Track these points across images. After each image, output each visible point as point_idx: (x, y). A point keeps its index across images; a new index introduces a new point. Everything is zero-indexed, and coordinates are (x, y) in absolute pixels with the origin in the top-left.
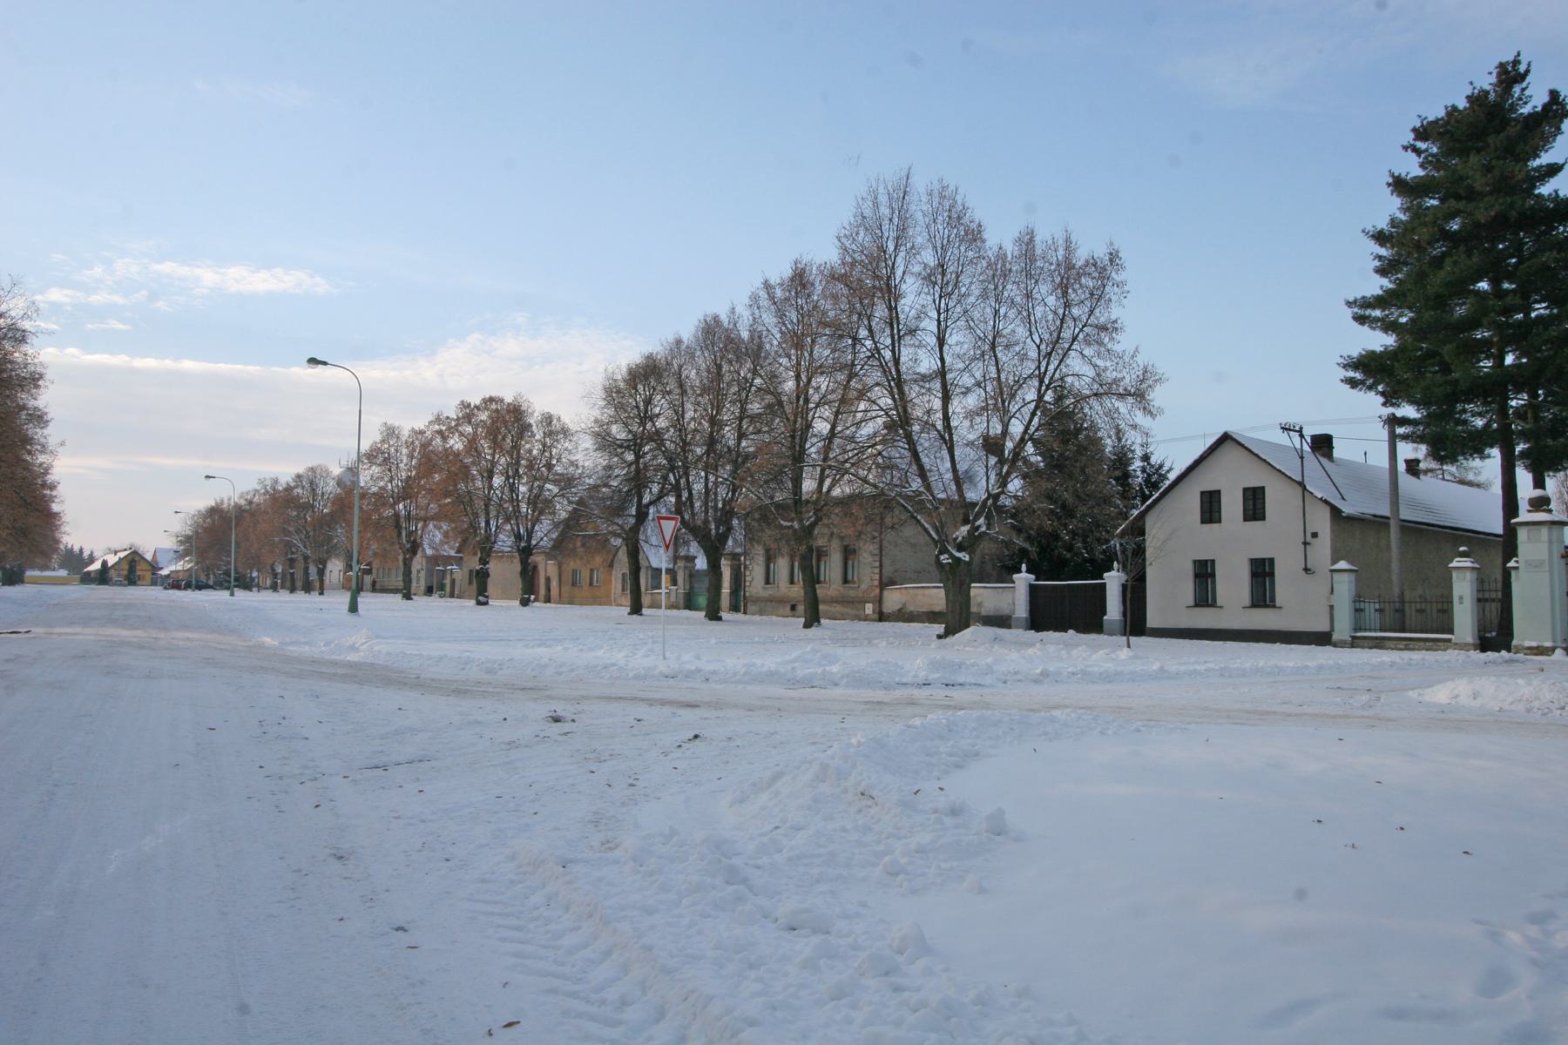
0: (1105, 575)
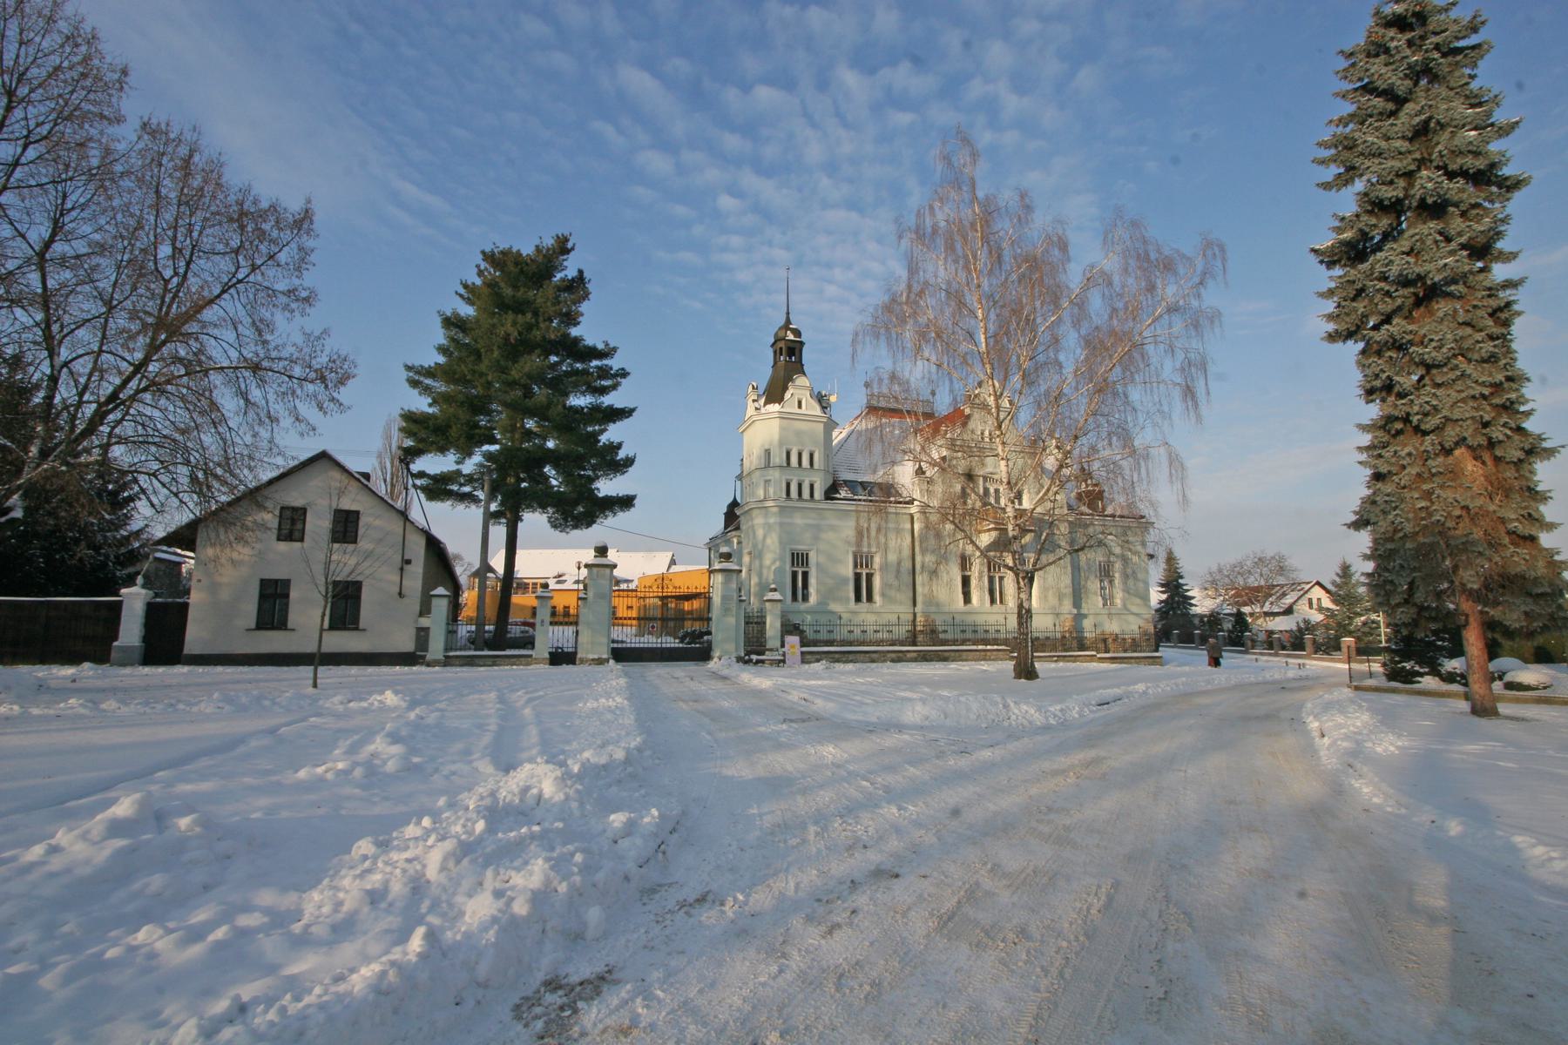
0: (124, 591)
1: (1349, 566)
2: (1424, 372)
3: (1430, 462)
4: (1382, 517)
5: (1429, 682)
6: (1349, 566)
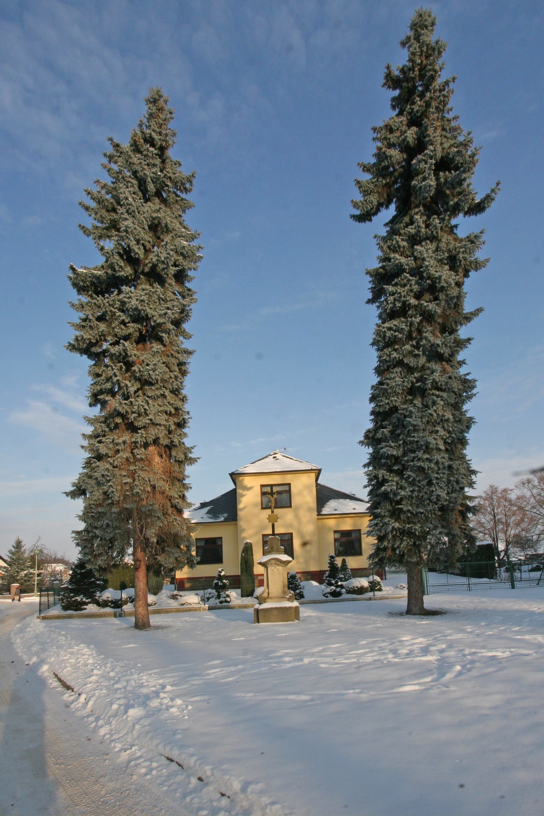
1: (21, 542)
2: (139, 386)
3: (135, 451)
4: (96, 488)
5: (91, 608)
6: (21, 542)
